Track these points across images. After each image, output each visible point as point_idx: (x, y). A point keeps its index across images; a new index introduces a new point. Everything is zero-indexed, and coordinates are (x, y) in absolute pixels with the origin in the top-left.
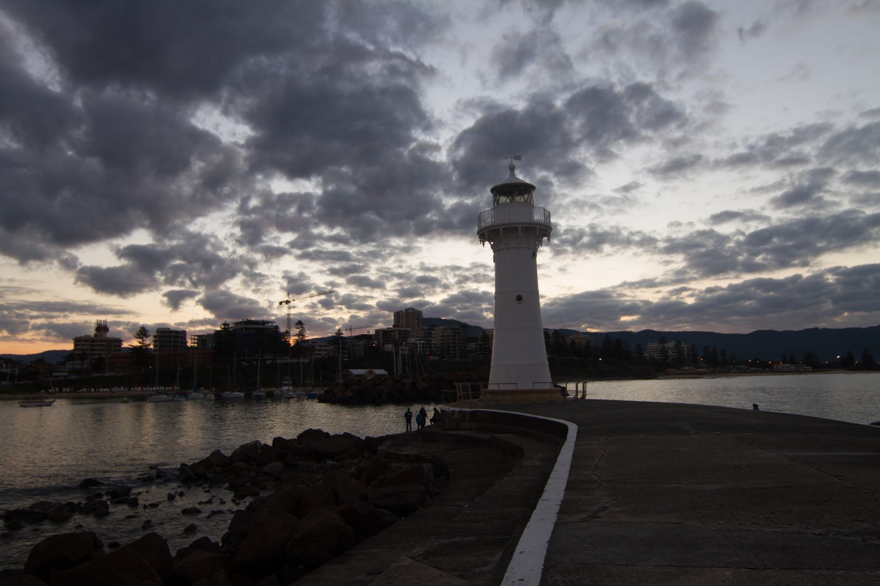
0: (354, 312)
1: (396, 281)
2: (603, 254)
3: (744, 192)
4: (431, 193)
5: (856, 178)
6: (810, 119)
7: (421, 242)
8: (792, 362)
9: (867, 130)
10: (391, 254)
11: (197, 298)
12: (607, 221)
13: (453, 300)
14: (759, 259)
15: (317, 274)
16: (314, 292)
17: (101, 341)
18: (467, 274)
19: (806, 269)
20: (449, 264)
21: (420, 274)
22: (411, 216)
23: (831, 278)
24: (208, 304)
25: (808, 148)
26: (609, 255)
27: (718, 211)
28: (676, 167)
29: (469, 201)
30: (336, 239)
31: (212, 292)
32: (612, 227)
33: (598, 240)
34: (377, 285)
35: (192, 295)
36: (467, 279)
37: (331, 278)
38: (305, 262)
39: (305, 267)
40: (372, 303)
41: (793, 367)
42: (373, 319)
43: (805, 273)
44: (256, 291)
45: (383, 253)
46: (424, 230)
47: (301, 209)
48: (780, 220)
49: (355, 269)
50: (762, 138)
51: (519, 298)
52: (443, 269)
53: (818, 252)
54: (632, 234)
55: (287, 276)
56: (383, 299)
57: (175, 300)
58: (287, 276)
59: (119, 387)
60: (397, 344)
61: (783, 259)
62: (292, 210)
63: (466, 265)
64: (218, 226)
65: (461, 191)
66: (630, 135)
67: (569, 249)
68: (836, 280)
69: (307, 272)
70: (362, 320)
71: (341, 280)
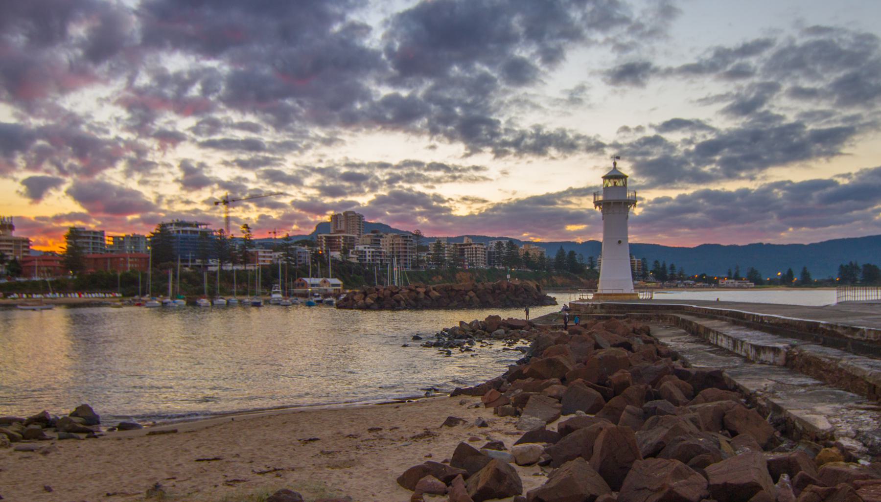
0: (265, 211)
1: (319, 177)
2: (547, 158)
3: (691, 102)
4: (359, 80)
5: (798, 93)
6: (752, 35)
7: (345, 135)
8: (737, 278)
9: (805, 48)
10: (308, 147)
11: (64, 188)
12: (552, 124)
13: (381, 201)
14: (707, 169)
15: (220, 167)
16: (216, 186)
17: (7, 241)
18: (398, 172)
19: (754, 182)
20: (377, 160)
21: (344, 170)
22: (335, 106)
23: (780, 194)
24: (78, 194)
25: (753, 61)
26: (553, 158)
27: (668, 118)
28: (630, 73)
29: (404, 93)
30: (243, 126)
31: (86, 180)
32: (558, 129)
33: (540, 144)
34: (294, 180)
35: (55, 183)
36: (397, 178)
37: (238, 172)
38: (209, 151)
39: (209, 157)
40: (287, 201)
41: (737, 283)
42: (288, 220)
43: (752, 186)
44: (143, 183)
45: (300, 145)
46: (351, 121)
47: (206, 91)
48: (727, 130)
49: (267, 162)
50: (709, 49)
51: (620, 242)
52: (370, 166)
53: (764, 165)
54: (578, 137)
55: (185, 166)
56: (300, 198)
57: (36, 190)
58: (185, 166)
59: (60, 293)
60: (345, 252)
61: (731, 169)
62: (195, 91)
63: (395, 162)
64: (97, 105)
65: (394, 82)
66: (574, 35)
67: (513, 150)
68: (784, 194)
69: (209, 163)
70: (274, 221)
71: (250, 175)
